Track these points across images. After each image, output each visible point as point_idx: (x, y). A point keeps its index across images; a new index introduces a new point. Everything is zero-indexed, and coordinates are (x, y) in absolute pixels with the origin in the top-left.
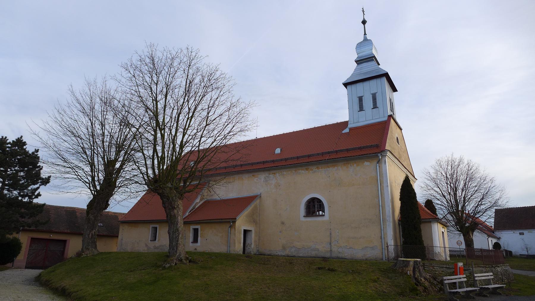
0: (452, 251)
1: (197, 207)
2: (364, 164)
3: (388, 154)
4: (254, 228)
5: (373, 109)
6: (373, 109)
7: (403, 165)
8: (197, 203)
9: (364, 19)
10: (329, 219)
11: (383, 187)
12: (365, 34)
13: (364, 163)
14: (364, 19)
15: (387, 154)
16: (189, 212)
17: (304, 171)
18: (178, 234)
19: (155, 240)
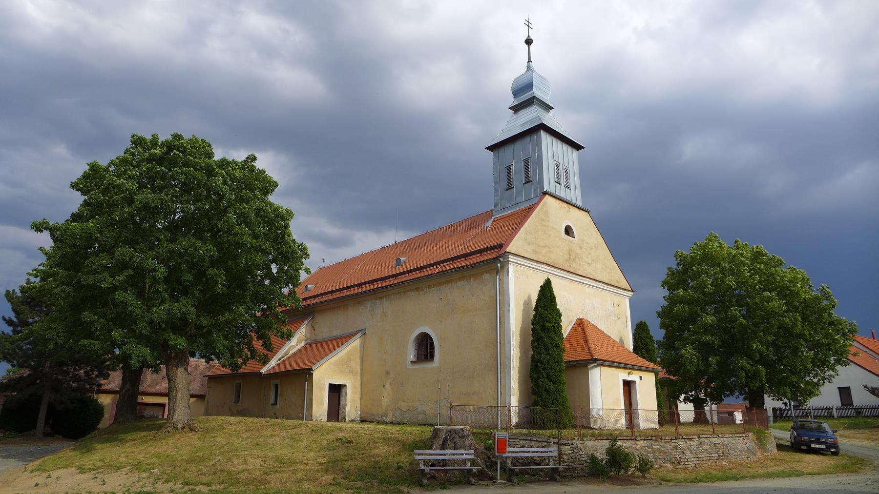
0: (823, 409)
1: (291, 352)
2: (483, 276)
3: (511, 258)
4: (350, 381)
5: (525, 183)
6: (525, 183)
7: (568, 272)
8: (292, 346)
9: (529, 36)
10: (438, 365)
11: (504, 311)
12: (529, 61)
13: (483, 274)
14: (529, 36)
15: (510, 259)
16: (278, 361)
17: (414, 291)
18: (175, 393)
19: (238, 401)
